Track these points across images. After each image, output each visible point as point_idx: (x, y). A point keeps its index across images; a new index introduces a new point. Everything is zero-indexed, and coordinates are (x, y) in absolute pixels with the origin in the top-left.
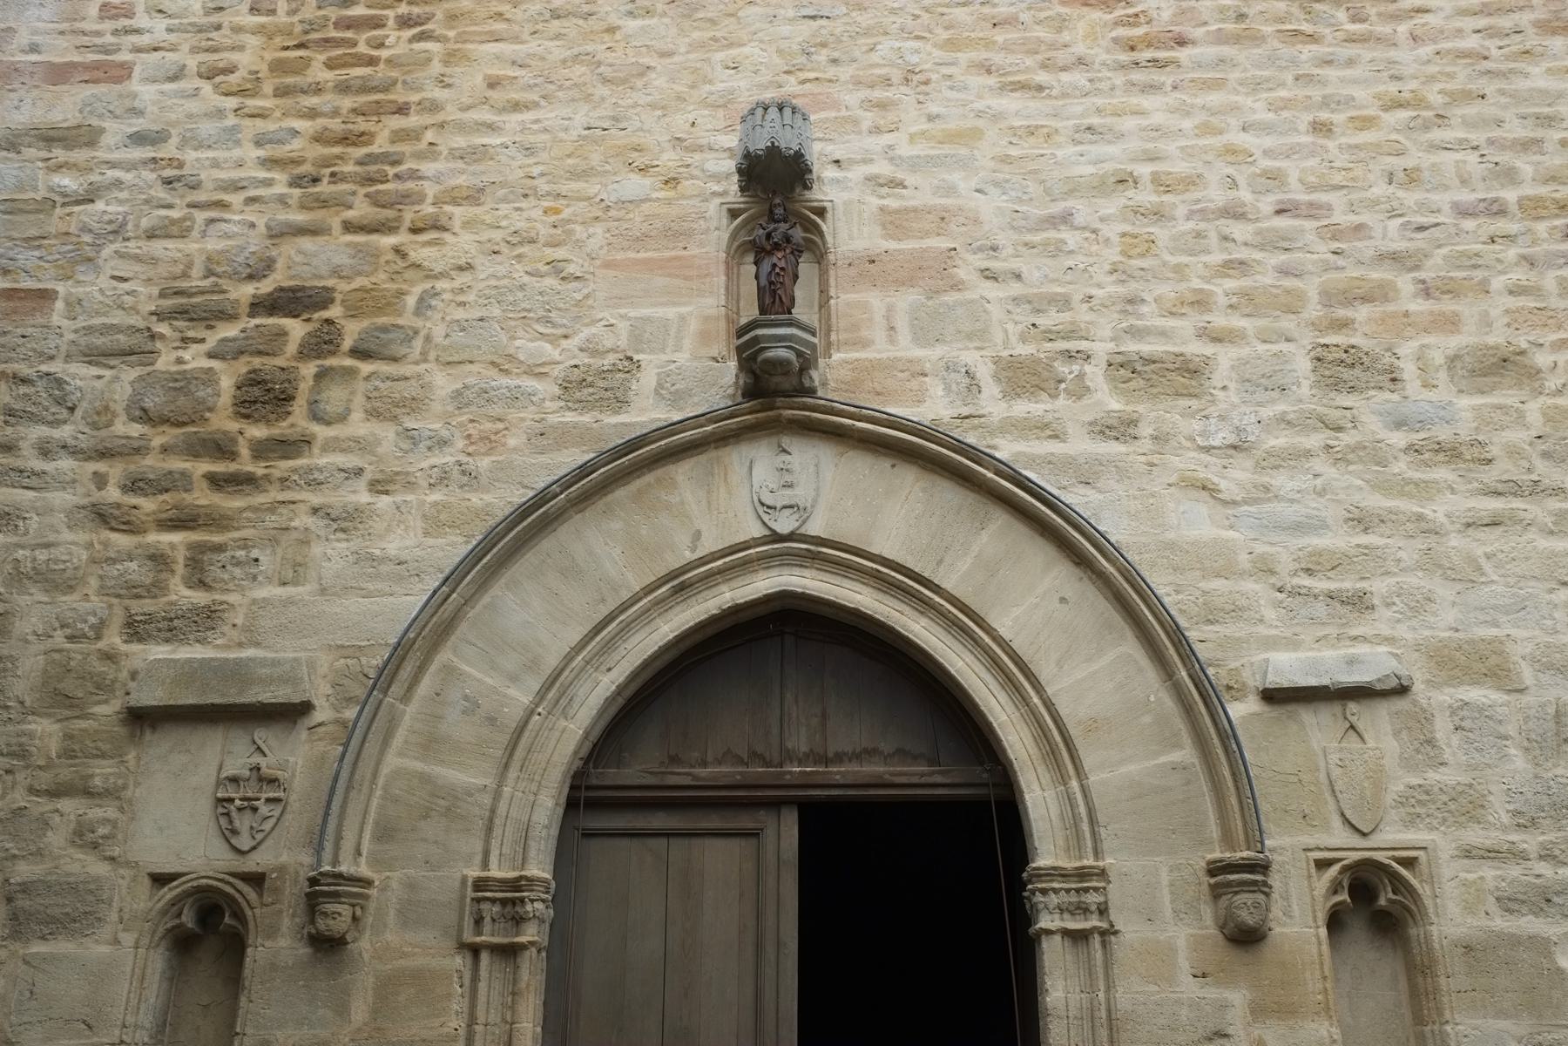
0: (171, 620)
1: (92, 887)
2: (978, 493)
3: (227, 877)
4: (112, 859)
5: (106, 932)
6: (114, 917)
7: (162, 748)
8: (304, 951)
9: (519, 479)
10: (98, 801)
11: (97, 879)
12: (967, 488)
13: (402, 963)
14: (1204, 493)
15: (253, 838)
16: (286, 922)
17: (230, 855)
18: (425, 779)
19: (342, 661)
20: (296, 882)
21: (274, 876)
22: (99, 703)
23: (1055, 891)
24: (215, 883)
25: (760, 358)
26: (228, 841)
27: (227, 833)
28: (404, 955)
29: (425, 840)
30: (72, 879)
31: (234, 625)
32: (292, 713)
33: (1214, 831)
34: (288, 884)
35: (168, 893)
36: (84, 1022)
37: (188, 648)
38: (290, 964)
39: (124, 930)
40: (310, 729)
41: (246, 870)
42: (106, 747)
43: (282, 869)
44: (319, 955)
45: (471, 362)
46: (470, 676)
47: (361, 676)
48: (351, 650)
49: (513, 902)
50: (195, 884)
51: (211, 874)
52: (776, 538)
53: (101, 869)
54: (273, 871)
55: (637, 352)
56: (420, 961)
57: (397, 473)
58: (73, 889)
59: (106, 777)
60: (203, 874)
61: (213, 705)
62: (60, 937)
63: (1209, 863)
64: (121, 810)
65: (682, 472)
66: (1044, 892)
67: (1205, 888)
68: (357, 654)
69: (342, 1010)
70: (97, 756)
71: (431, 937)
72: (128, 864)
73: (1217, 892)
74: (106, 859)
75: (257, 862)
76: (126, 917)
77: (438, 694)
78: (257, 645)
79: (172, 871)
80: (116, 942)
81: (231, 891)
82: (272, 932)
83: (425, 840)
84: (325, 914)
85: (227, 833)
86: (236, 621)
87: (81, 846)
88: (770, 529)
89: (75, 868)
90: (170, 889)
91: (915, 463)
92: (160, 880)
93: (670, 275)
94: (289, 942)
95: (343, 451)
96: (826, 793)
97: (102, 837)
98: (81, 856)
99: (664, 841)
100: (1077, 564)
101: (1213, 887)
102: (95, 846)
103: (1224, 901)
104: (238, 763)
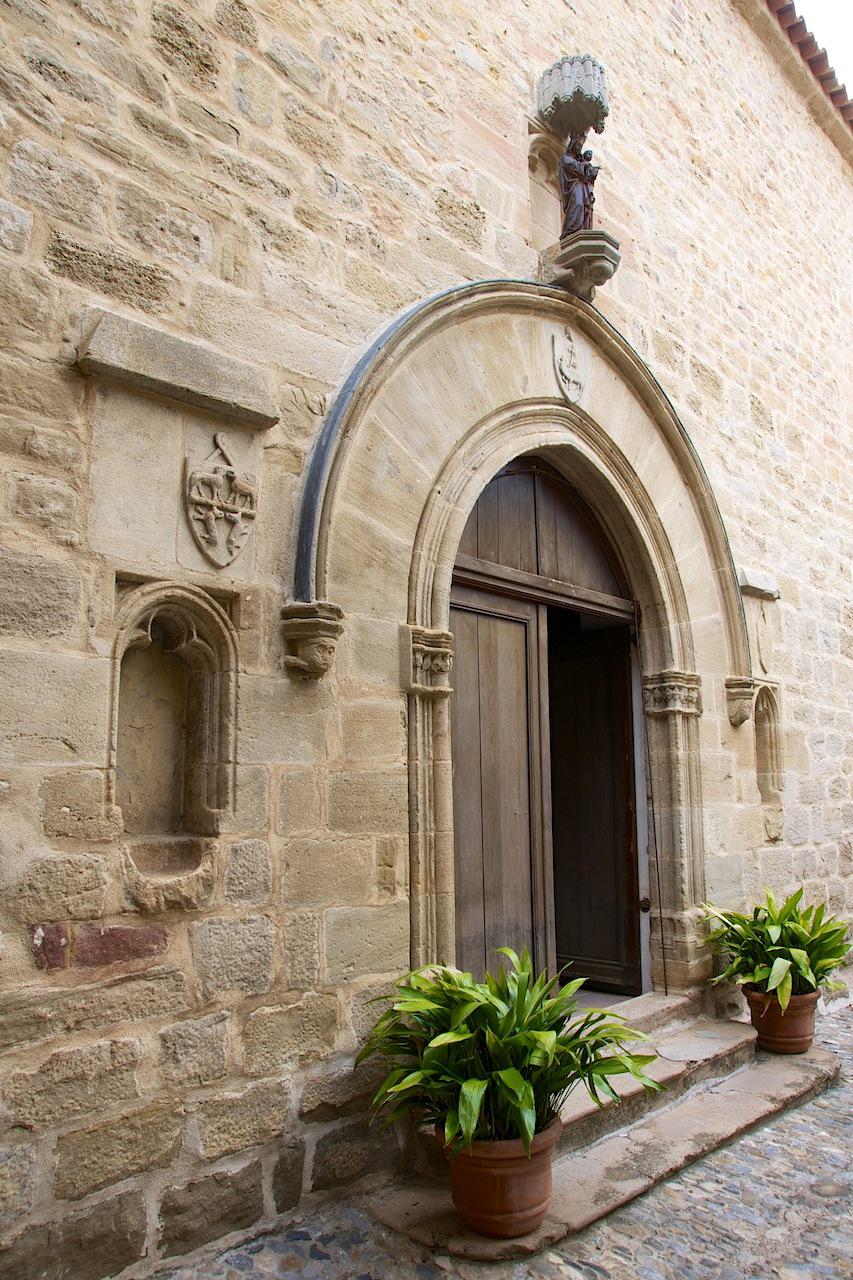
0: (109, 267)
1: (52, 576)
2: (650, 417)
3: (197, 589)
4: (70, 545)
5: (76, 634)
6: (82, 617)
7: (116, 419)
8: (283, 681)
9: (415, 272)
10: (40, 467)
11: (55, 567)
12: (646, 412)
13: (363, 701)
14: (720, 460)
15: (231, 553)
16: (263, 649)
17: (205, 568)
18: (366, 529)
19: (288, 386)
20: (269, 609)
21: (248, 598)
22: (30, 339)
23: (680, 688)
24: (191, 596)
25: (598, 263)
26: (200, 549)
27: (203, 542)
28: (364, 694)
29: (369, 587)
30: (24, 561)
31: (182, 304)
32: (252, 424)
33: (728, 662)
34: (261, 610)
35: (139, 601)
36: (65, 742)
37: (130, 310)
38: (272, 692)
39: (97, 635)
40: (266, 448)
41: (222, 587)
42: (46, 400)
43: (255, 592)
44: (295, 687)
45: (369, 137)
46: (391, 440)
47: (306, 408)
48: (296, 377)
49: (434, 656)
50: (169, 592)
51: (186, 584)
52: (564, 402)
53: (57, 555)
54: (248, 592)
55: (484, 205)
56: (374, 701)
57: (320, 213)
58: (28, 573)
59: (52, 439)
60: (178, 583)
61: (188, 390)
62: (17, 633)
63: (727, 680)
64: (74, 486)
65: (516, 320)
66: (673, 688)
67: (725, 693)
68: (301, 384)
69: (319, 742)
70: (35, 409)
71: (382, 679)
72: (91, 555)
73: (731, 698)
74: (60, 543)
75: (226, 581)
76: (98, 620)
77: (369, 449)
78: (208, 337)
79: (144, 573)
80: (89, 648)
81: (206, 606)
82: (252, 658)
83: (369, 587)
84: (324, 647)
85: (203, 542)
86: (185, 301)
87: (26, 520)
88: (563, 394)
89: (22, 546)
90: (143, 595)
91: (625, 382)
92: (126, 582)
93: (498, 152)
94: (269, 670)
95: (270, 160)
96: (571, 602)
97: (55, 515)
98: (27, 533)
99: (475, 617)
100: (686, 484)
101: (729, 694)
102: (45, 524)
103: (737, 703)
104: (205, 465)
